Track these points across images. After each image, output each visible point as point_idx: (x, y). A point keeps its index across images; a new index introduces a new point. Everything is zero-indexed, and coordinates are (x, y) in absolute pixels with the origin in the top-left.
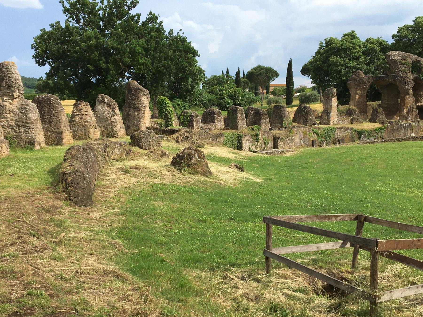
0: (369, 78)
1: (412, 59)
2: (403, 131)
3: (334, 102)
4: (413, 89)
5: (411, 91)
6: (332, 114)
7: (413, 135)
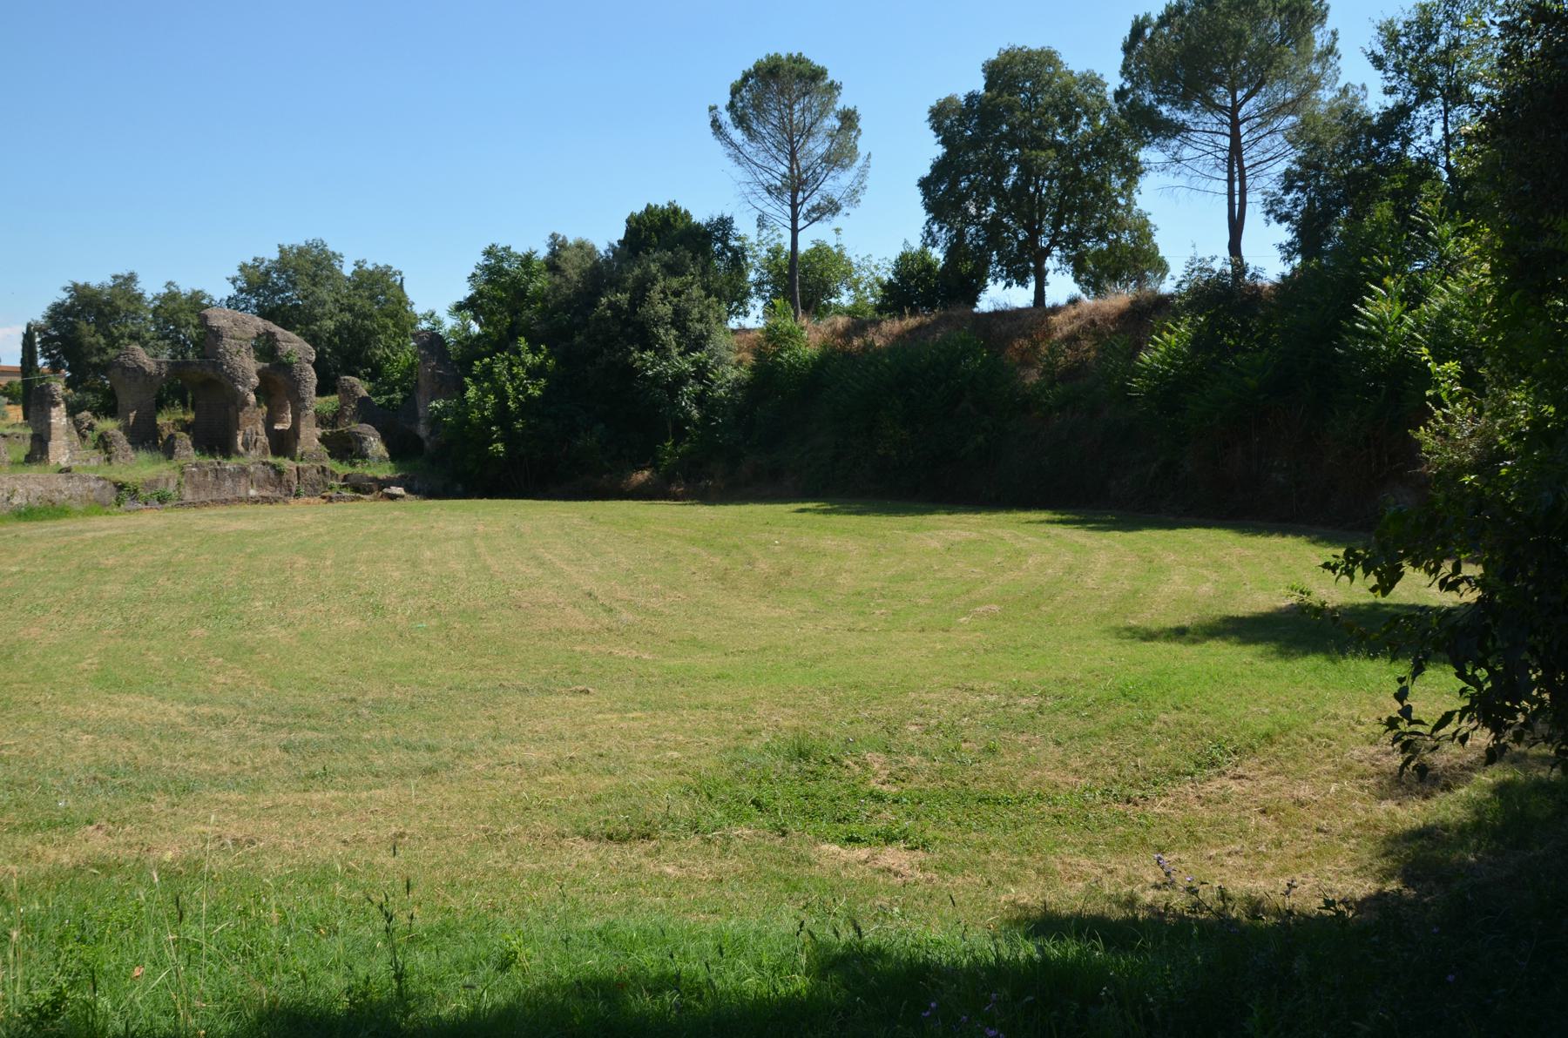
0: (159, 364)
1: (257, 328)
2: (228, 483)
3: (59, 417)
4: (257, 392)
5: (252, 398)
6: (52, 444)
7: (252, 492)
